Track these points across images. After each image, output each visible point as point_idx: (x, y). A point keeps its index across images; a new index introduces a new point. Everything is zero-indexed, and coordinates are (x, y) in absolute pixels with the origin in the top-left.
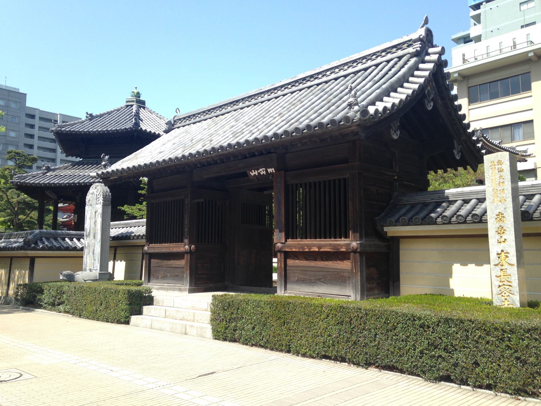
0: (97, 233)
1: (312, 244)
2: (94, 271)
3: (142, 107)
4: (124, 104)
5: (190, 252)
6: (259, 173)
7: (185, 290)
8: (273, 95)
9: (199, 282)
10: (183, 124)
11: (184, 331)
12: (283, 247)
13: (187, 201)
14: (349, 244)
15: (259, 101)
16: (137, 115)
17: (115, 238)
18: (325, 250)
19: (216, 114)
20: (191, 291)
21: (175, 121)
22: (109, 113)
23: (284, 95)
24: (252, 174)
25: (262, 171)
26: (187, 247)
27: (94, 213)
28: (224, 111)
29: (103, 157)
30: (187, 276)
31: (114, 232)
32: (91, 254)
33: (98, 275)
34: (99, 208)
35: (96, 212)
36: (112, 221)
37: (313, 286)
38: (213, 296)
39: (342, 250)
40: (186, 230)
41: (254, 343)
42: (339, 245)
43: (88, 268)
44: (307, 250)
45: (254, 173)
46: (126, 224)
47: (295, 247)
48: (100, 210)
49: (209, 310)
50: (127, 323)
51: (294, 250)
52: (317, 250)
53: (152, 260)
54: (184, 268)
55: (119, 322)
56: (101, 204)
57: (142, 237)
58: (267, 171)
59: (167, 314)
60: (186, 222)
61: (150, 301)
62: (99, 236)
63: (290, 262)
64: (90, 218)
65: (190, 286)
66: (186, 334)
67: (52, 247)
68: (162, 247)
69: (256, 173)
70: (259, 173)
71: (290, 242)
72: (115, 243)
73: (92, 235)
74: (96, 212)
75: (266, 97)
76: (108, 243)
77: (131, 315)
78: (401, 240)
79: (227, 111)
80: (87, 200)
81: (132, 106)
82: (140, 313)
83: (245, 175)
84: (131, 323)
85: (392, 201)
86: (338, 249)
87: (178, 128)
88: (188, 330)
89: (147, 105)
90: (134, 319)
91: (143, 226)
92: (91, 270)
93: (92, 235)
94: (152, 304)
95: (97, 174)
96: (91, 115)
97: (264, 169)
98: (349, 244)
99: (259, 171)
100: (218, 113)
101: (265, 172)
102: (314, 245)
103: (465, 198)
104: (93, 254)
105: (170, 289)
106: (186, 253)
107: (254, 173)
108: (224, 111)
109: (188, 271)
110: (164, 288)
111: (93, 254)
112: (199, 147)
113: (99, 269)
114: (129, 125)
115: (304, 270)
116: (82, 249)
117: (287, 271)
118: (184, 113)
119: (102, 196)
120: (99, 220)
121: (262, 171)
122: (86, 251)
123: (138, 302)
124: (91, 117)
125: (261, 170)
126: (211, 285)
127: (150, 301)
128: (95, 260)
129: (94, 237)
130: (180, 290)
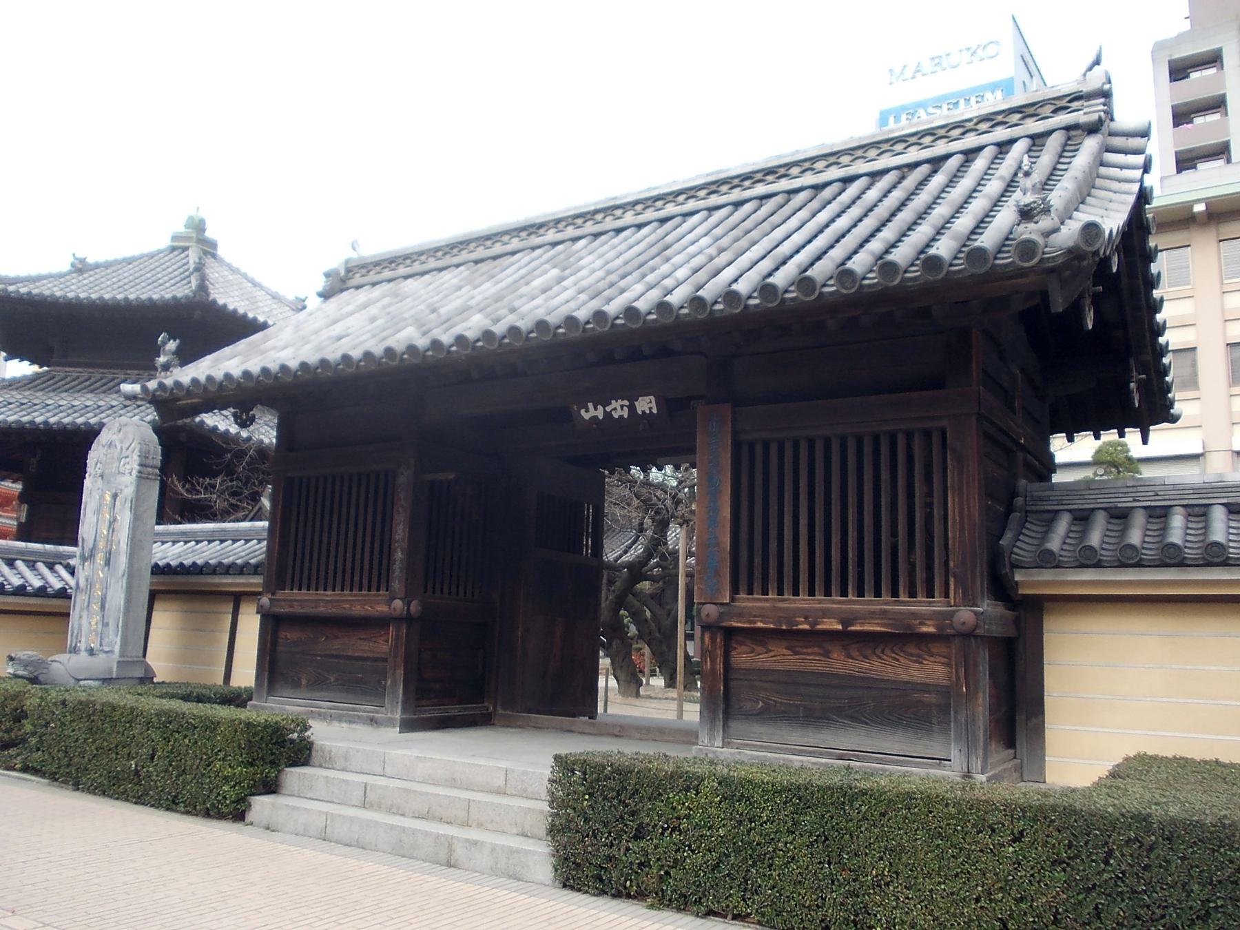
0: (118, 551)
1: (822, 610)
2: (102, 656)
3: (210, 253)
4: (165, 242)
5: (408, 619)
6: (607, 415)
7: (390, 723)
8: (650, 215)
9: (423, 702)
10: (372, 277)
11: (443, 856)
12: (721, 616)
13: (404, 478)
14: (951, 615)
15: (568, 237)
16: (199, 268)
17: (157, 570)
18: (867, 628)
19: (474, 256)
20: (409, 725)
21: (348, 271)
22: (129, 261)
23: (640, 226)
24: (586, 416)
25: (619, 409)
26: (398, 603)
27: (108, 498)
28: (498, 249)
29: (164, 343)
30: (394, 683)
31: (169, 553)
32: (96, 607)
33: (115, 666)
34: (127, 484)
35: (115, 496)
36: (157, 524)
37: (816, 727)
38: (557, 758)
39: (924, 629)
40: (399, 555)
41: (715, 907)
42: (914, 615)
43: (82, 646)
44: (806, 627)
45: (646, 404)
46: (184, 533)
47: (763, 618)
48: (129, 491)
49: (544, 795)
50: (239, 816)
51: (760, 625)
52: (840, 627)
53: (282, 634)
54: (385, 660)
55: (213, 812)
56: (135, 473)
57: (256, 569)
58: (632, 409)
59: (371, 796)
60: (400, 532)
61: (302, 754)
62: (122, 561)
63: (743, 657)
64: (98, 512)
65: (404, 710)
66: (450, 865)
67: (23, 587)
68: (317, 601)
69: (600, 413)
70: (607, 415)
71: (745, 602)
72: (165, 581)
73: (100, 559)
74: (115, 496)
75: (629, 218)
76: (146, 582)
77: (254, 795)
78: (1046, 604)
79: (509, 248)
80: (90, 462)
81: (185, 249)
82: (271, 787)
83: (564, 416)
84: (250, 817)
85: (1019, 501)
86: (910, 626)
87: (358, 287)
88: (460, 852)
89: (220, 252)
90: (261, 805)
91: (260, 541)
92: (91, 652)
93: (100, 559)
94: (306, 763)
95: (144, 388)
96: (83, 261)
97: (626, 403)
98: (951, 615)
99: (608, 409)
100: (481, 252)
101: (625, 414)
102: (826, 614)
103: (1231, 500)
104: (103, 607)
105: (340, 719)
106: (397, 620)
107: (646, 404)
108: (498, 249)
109: (400, 672)
110: (320, 714)
111: (103, 607)
112: (473, 326)
113: (117, 649)
114: (184, 291)
115: (788, 681)
116: (63, 594)
117: (732, 683)
118: (373, 248)
119: (137, 452)
120: (125, 519)
121: (619, 409)
122: (79, 600)
123: (275, 756)
124: (81, 268)
125: (614, 404)
126: (453, 710)
127: (302, 754)
128: (106, 625)
129: (108, 562)
130: (373, 721)
